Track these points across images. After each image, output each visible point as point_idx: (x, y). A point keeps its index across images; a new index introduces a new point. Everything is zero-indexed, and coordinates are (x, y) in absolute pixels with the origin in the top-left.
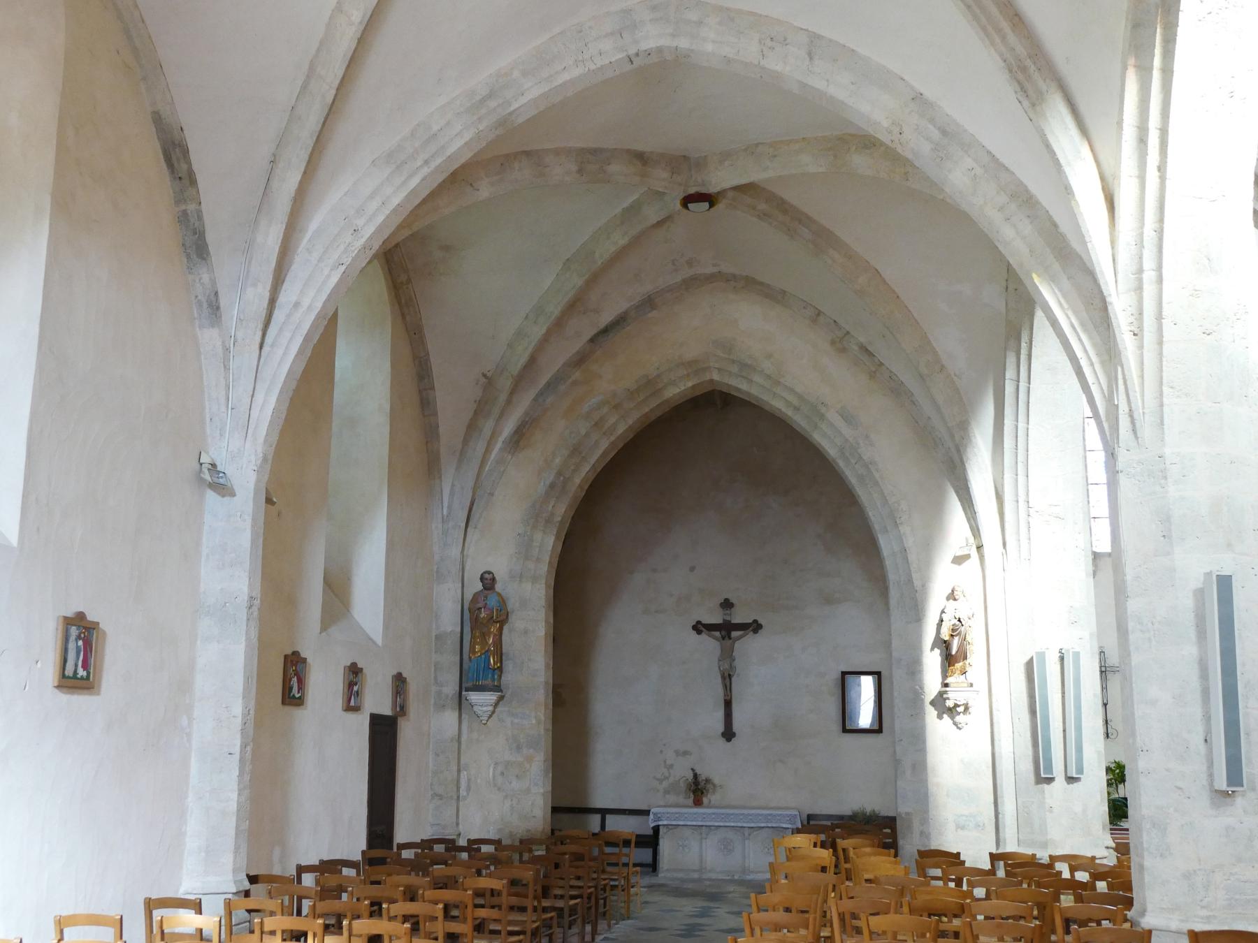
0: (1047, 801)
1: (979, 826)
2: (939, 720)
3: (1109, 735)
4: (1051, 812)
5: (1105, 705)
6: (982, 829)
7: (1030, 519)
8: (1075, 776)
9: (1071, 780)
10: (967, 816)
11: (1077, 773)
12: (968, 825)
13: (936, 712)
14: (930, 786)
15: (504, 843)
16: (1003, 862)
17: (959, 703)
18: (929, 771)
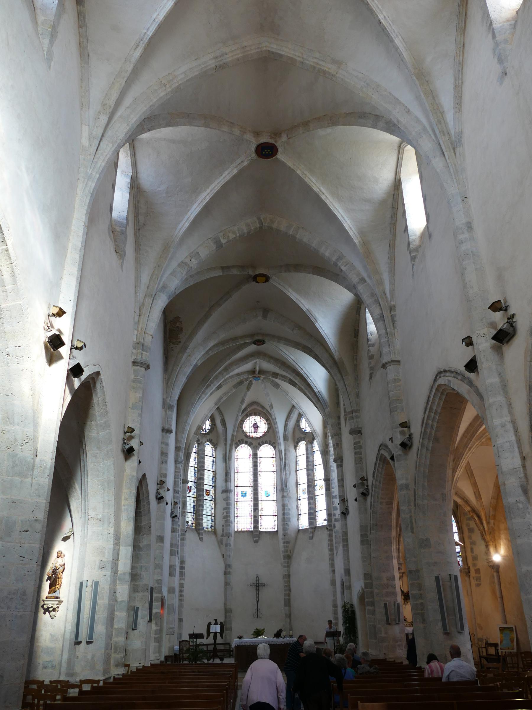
0: (76, 653)
1: (53, 666)
2: (44, 615)
3: (259, 616)
4: (78, 658)
5: (258, 602)
6: (54, 668)
7: (89, 521)
8: (460, 631)
9: (88, 643)
10: (48, 662)
11: (461, 630)
12: (48, 666)
13: (43, 611)
14: (34, 647)
15: (45, 683)
16: (100, 685)
17: (49, 606)
18: (35, 639)
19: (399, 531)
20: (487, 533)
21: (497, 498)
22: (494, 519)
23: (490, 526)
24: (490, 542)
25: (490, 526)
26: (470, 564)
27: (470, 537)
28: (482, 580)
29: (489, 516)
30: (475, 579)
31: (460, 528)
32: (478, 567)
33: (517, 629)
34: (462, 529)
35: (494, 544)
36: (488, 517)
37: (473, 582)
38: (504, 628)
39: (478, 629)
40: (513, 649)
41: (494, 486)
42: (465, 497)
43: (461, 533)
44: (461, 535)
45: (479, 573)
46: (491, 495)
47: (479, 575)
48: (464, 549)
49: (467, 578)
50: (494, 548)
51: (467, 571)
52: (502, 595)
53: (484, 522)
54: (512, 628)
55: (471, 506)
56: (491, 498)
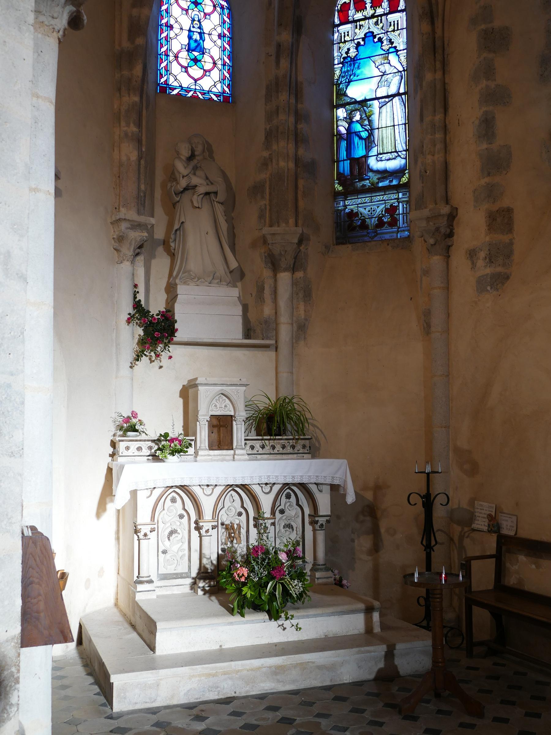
31: (438, 43)
32: (506, 202)
51: (443, 222)
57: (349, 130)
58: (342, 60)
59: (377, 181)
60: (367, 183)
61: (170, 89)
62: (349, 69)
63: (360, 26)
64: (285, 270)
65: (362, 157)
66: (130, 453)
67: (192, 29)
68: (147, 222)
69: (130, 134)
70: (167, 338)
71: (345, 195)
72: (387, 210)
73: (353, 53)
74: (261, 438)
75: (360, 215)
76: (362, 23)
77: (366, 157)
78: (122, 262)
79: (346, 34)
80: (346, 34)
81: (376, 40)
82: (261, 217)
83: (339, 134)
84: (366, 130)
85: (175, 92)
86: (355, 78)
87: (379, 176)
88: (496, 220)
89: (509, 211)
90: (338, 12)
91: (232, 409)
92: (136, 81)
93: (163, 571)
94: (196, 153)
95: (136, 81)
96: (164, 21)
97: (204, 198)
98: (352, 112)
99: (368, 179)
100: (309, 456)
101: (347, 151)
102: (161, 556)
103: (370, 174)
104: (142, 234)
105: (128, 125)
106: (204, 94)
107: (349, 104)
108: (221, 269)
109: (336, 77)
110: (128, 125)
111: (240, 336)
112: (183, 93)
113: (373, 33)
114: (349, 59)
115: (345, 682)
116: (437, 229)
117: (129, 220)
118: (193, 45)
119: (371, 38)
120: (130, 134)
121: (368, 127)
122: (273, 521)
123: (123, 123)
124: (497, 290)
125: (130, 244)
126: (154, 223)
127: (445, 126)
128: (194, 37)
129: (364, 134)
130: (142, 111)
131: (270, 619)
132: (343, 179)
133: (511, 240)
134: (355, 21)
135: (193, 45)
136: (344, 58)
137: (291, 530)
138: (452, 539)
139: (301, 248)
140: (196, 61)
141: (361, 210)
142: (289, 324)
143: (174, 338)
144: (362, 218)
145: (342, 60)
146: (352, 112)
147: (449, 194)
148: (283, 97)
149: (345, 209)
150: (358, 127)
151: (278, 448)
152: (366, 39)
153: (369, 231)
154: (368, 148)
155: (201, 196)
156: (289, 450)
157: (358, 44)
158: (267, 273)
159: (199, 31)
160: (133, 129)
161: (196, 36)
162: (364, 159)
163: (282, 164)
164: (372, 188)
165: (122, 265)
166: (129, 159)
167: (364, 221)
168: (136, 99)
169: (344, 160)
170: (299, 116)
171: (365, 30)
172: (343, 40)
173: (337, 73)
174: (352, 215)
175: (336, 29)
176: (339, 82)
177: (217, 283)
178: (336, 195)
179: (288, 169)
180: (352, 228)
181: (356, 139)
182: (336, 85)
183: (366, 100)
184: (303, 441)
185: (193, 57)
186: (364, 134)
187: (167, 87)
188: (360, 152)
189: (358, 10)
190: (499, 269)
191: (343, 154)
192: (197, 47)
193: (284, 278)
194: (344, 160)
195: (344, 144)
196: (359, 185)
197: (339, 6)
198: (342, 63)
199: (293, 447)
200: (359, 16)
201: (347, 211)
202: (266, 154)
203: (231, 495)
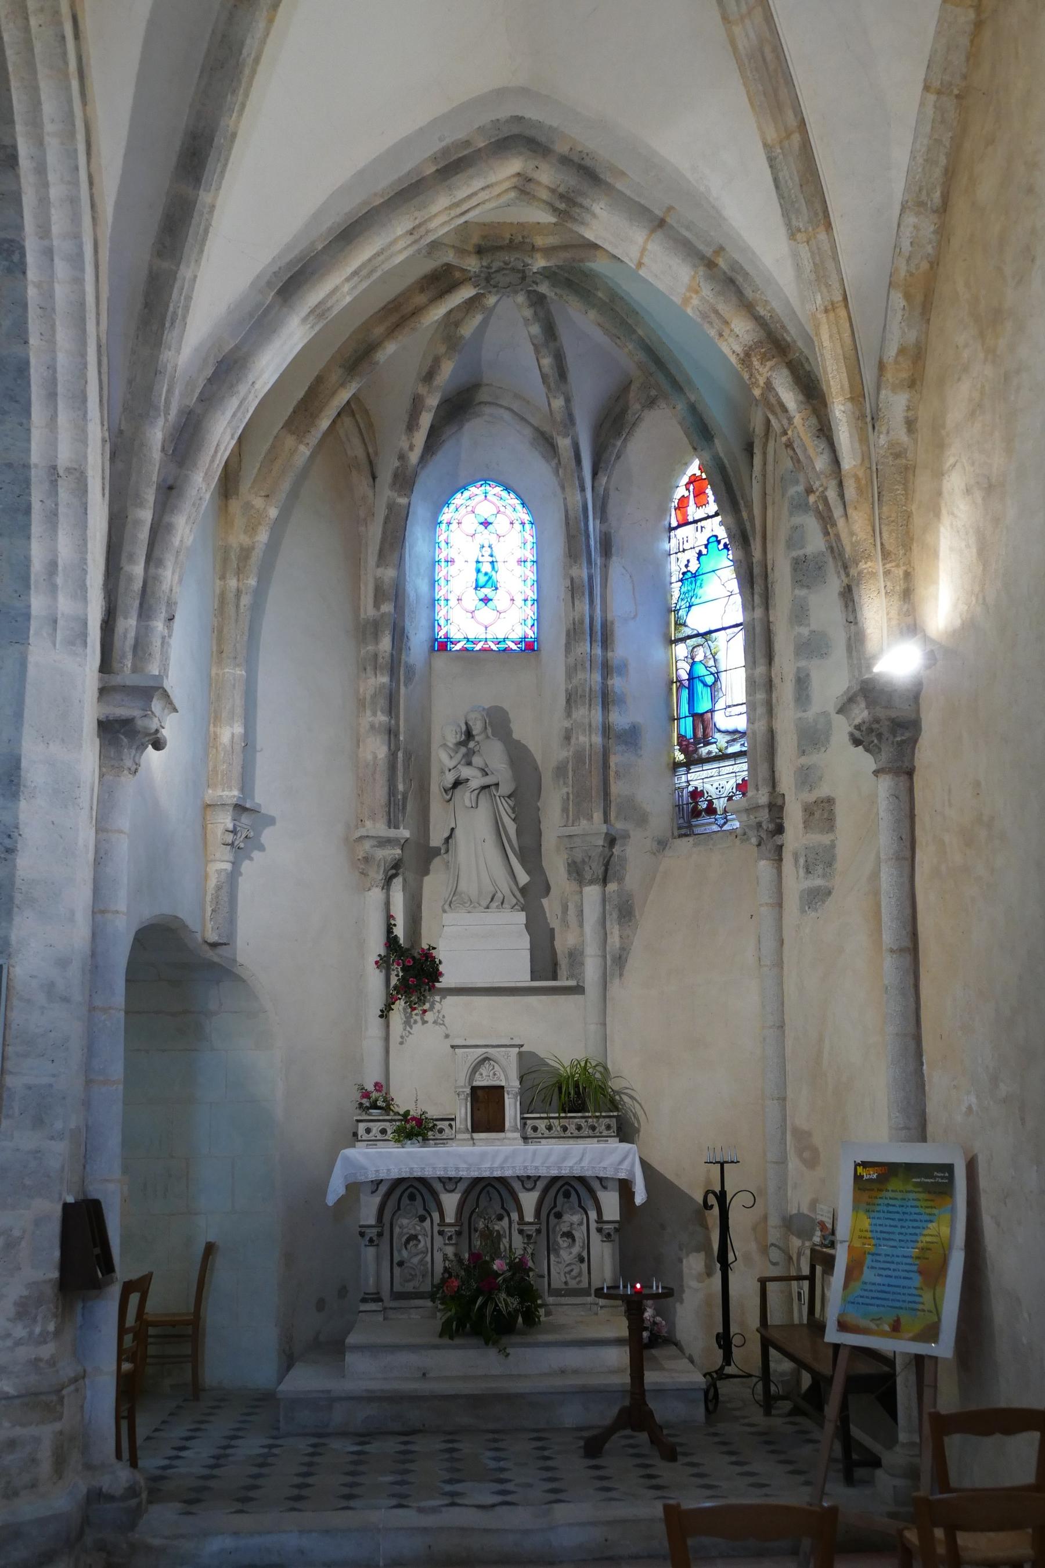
19: (156, 455)
20: (850, 491)
21: (946, 198)
22: (913, 383)
23: (883, 440)
24: (869, 558)
25: (883, 440)
26: (787, 783)
27: (800, 614)
28: (839, 865)
29: (881, 367)
30: (802, 861)
31: (757, 570)
32: (824, 791)
33: (983, 1183)
34: (766, 577)
35: (900, 572)
36: (869, 376)
37: (795, 882)
38: (889, 1171)
39: (794, 1163)
40: (931, 1333)
41: (927, 88)
42: (720, 250)
43: (757, 599)
44: (759, 613)
45: (829, 823)
46: (898, 189)
47: (825, 839)
48: (760, 696)
49: (763, 864)
50: (896, 603)
51: (764, 815)
52: (914, 935)
53: (840, 411)
54: (948, 1169)
55: (761, 311)
56: (903, 209)
57: (690, 673)
58: (681, 576)
59: (726, 745)
60: (713, 748)
61: (452, 643)
62: (689, 588)
63: (702, 527)
64: (591, 882)
65: (707, 712)
66: (371, 1136)
67: (481, 559)
68: (399, 836)
69: (377, 726)
70: (428, 984)
71: (688, 764)
72: (738, 787)
73: (693, 567)
74: (545, 1115)
75: (706, 795)
76: (703, 523)
77: (712, 711)
78: (369, 890)
79: (685, 540)
80: (685, 540)
81: (721, 546)
82: (565, 810)
83: (679, 681)
84: (712, 674)
85: (458, 647)
86: (697, 601)
87: (728, 738)
88: (814, 814)
89: (830, 801)
90: (675, 510)
91: (503, 1077)
92: (383, 658)
93: (397, 1288)
94: (474, 733)
95: (383, 658)
96: (442, 556)
97: (481, 794)
98: (694, 648)
99: (715, 743)
100: (617, 1139)
101: (689, 704)
102: (397, 1270)
103: (718, 735)
104: (393, 851)
105: (374, 714)
106: (499, 643)
107: (690, 637)
108: (504, 885)
109: (674, 601)
110: (374, 714)
111: (529, 977)
112: (469, 646)
113: (716, 536)
114: (689, 574)
115: (567, 1426)
116: (759, 825)
117: (373, 837)
118: (482, 581)
119: (716, 543)
120: (377, 726)
121: (713, 670)
122: (537, 1226)
123: (368, 713)
124: (816, 910)
125: (379, 866)
126: (408, 836)
127: (771, 681)
128: (483, 570)
129: (710, 680)
130: (399, 688)
131: (487, 1343)
132: (684, 743)
133: (832, 841)
134: (695, 522)
135: (482, 579)
136: (684, 574)
137: (570, 1240)
138: (790, 1258)
139: (614, 850)
140: (486, 600)
141: (707, 787)
142: (11, 1073)
143: (437, 985)
144: (709, 798)
145: (681, 576)
146: (694, 648)
147: (777, 775)
148: (584, 647)
149: (687, 787)
150: (700, 670)
151: (572, 1128)
152: (710, 546)
153: (717, 816)
154: (714, 699)
155: (476, 792)
156: (586, 1131)
157: (700, 554)
158: (573, 886)
159: (490, 559)
160: (382, 718)
161: (486, 567)
162: (709, 715)
163: (583, 739)
164: (720, 756)
165: (370, 893)
166: (375, 757)
167: (710, 803)
168: (384, 679)
169: (685, 717)
170: (607, 669)
171: (707, 533)
172: (681, 550)
173: (676, 594)
174: (696, 794)
175: (672, 534)
176: (678, 607)
177: (497, 907)
178: (676, 766)
179: (591, 745)
180: (696, 813)
181: (699, 687)
182: (674, 611)
183: (710, 632)
184: (607, 1120)
185: (482, 596)
186: (710, 680)
187: (447, 642)
188: (703, 705)
189: (698, 506)
190: (819, 882)
191: (685, 710)
192: (487, 581)
193: (592, 893)
194: (685, 717)
195: (685, 693)
196: (704, 751)
197: (677, 501)
198: (681, 580)
199: (593, 1128)
200: (700, 513)
201: (691, 789)
202: (567, 724)
203: (488, 1191)
